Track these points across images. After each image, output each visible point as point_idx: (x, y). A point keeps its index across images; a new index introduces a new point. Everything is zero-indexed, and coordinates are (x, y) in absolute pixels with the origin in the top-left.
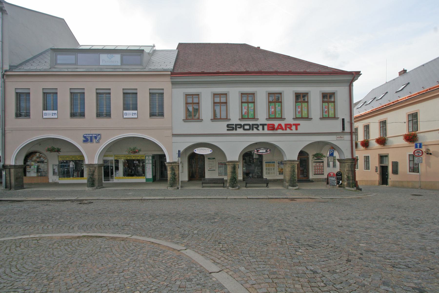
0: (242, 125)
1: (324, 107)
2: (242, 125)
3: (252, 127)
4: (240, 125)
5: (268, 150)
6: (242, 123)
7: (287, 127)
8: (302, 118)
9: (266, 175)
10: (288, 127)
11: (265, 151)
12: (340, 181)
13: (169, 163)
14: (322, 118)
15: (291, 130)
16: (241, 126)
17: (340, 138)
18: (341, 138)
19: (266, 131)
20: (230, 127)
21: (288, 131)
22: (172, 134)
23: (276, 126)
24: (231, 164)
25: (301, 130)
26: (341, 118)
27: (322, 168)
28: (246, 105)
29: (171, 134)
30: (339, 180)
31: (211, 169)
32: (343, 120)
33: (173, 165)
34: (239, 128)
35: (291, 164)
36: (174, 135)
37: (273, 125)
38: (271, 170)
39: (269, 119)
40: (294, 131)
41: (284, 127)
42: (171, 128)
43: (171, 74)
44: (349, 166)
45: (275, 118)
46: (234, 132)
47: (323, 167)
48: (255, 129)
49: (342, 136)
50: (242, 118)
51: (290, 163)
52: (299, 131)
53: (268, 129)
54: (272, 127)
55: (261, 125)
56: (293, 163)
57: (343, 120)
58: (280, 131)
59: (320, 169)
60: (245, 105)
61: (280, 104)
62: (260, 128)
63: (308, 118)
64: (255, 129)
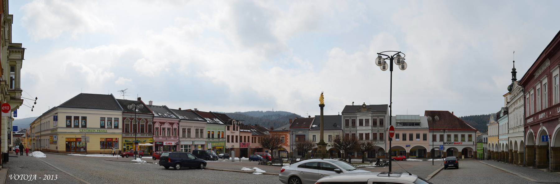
3: (450, 143)
8: (463, 141)
16: (447, 143)
21: (459, 144)
36: (429, 145)
39: (454, 141)
40: (461, 144)
50: (447, 141)
52: (462, 144)
54: (455, 143)
58: (457, 144)
62: (452, 143)
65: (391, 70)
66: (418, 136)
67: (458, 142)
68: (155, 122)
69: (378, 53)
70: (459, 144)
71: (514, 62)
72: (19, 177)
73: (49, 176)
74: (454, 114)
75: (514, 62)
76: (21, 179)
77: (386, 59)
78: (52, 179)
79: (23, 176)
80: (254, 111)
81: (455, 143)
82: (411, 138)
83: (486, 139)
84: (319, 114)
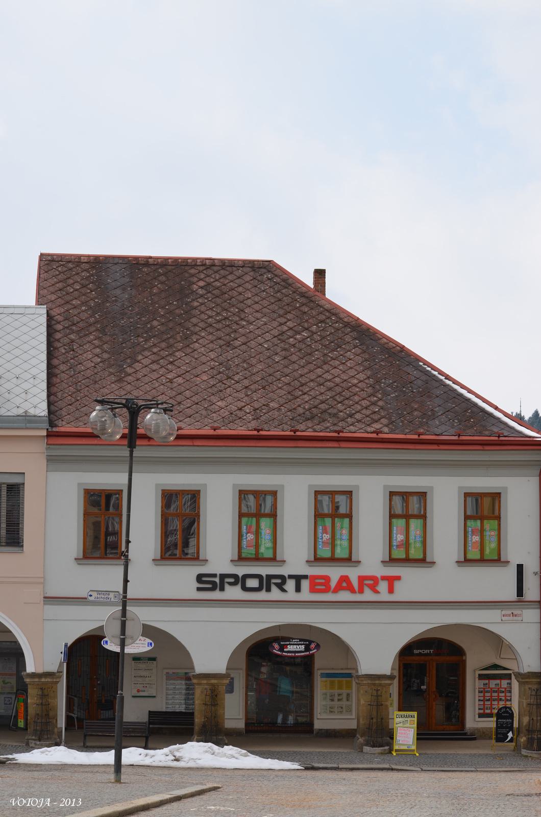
0: (240, 576)
1: (244, 528)
2: (240, 576)
3: (266, 583)
4: (235, 576)
5: (313, 646)
6: (241, 571)
7: (365, 584)
8: (407, 561)
9: (325, 716)
10: (368, 585)
11: (302, 648)
12: (508, 732)
13: (33, 675)
14: (466, 561)
15: (377, 592)
16: (239, 581)
17: (511, 618)
18: (515, 618)
19: (306, 594)
20: (207, 582)
21: (368, 595)
22: (45, 597)
23: (333, 584)
24: (205, 682)
25: (402, 592)
26: (515, 560)
27: (505, 696)
28: (401, 523)
29: (43, 596)
30: (504, 731)
31: (141, 694)
32: (520, 568)
33: (43, 680)
34: (230, 584)
35: (374, 684)
36: (50, 600)
37: (327, 579)
38: (339, 700)
39: (317, 560)
40: (384, 596)
41: (355, 583)
42: (42, 580)
43: (48, 436)
44: (534, 693)
45: (333, 560)
46: (216, 595)
47: (510, 692)
48: (274, 588)
49: (515, 612)
50: (241, 559)
51: (369, 682)
52: (400, 595)
53: (313, 590)
54: (320, 584)
55: (291, 577)
56: (377, 682)
57: (520, 568)
58: (344, 596)
59: (501, 700)
60: (400, 523)
61: (496, 522)
62: (290, 585)
63: (423, 561)
64: (274, 588)
67: (353, 574)
70: (368, 595)
72: (24, 801)
73: (67, 804)
74: (335, 293)
76: (28, 805)
78: (73, 805)
79: (31, 800)
80: (284, 761)
81: (320, 584)
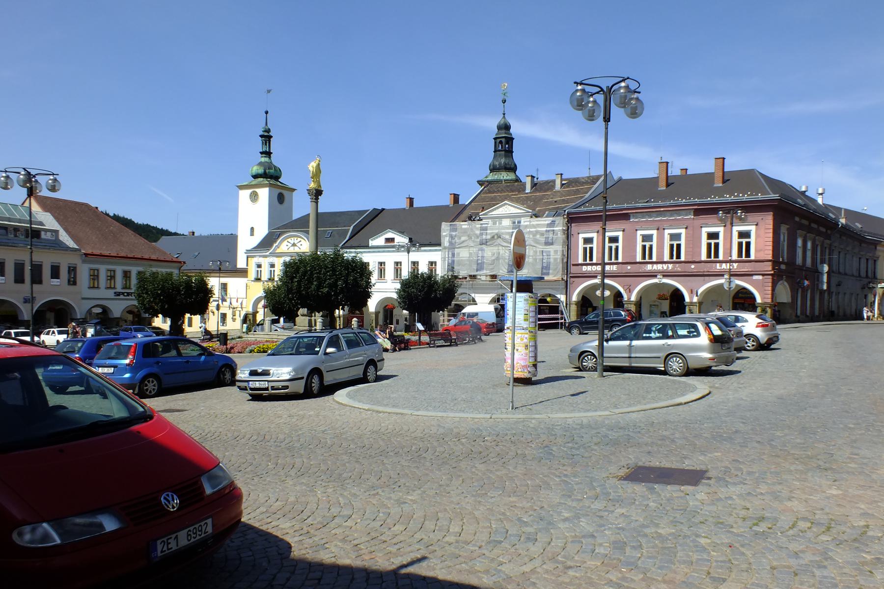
65: (607, 119)
66: (55, 273)
68: (562, 279)
69: (575, 83)
71: (267, 113)
75: (267, 113)
77: (598, 93)
82: (37, 278)
83: (28, 268)
84: (770, 263)
